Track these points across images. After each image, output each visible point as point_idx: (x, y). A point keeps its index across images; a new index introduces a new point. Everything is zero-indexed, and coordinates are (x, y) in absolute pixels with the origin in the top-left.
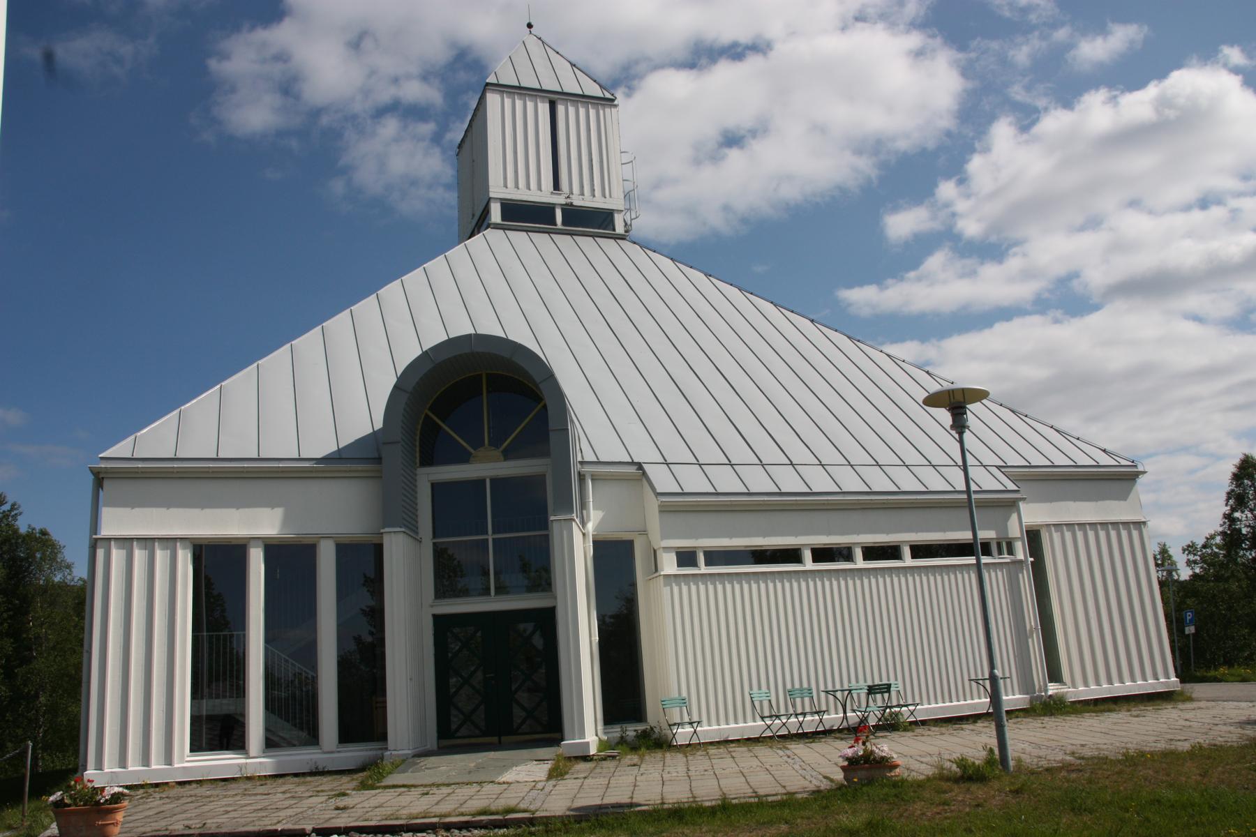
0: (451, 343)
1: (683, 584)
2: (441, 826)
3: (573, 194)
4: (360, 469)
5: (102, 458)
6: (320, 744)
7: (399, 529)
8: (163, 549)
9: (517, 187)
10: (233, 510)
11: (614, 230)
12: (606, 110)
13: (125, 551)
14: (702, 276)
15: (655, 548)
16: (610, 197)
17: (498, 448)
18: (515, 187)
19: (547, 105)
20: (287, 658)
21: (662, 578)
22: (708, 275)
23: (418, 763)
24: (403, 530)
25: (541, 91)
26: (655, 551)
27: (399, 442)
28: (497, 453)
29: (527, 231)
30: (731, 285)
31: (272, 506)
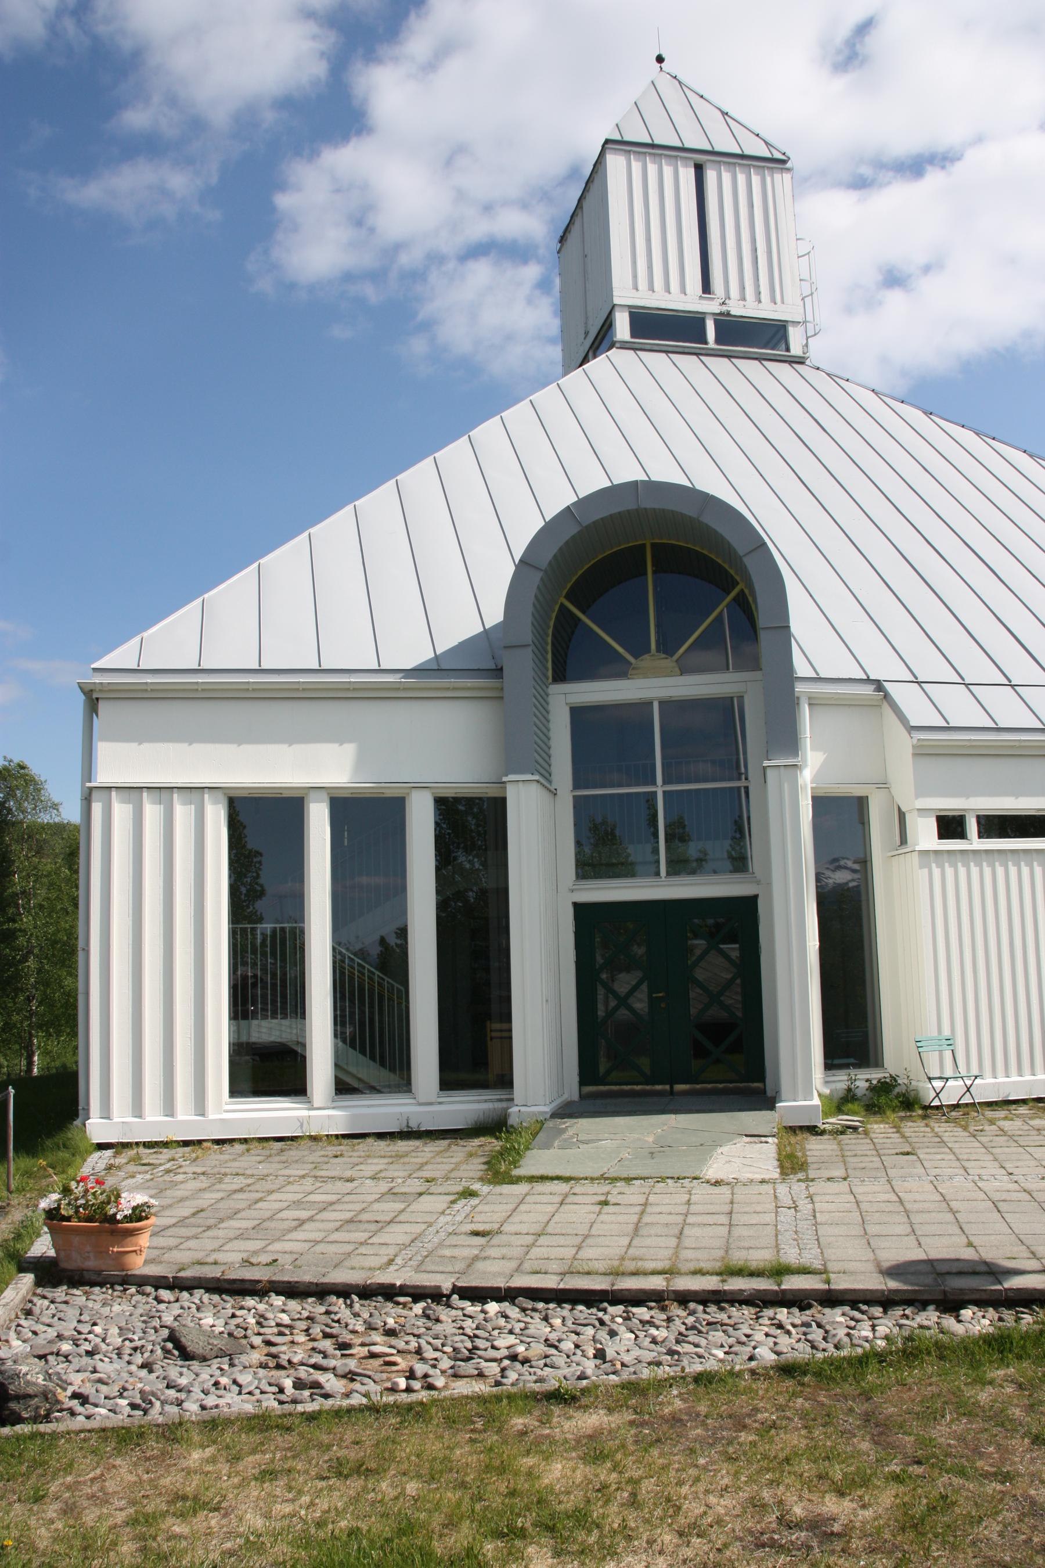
0: (583, 503)
1: (947, 865)
2: (672, 1296)
3: (729, 299)
4: (469, 685)
5: (95, 670)
6: (414, 1090)
7: (529, 777)
8: (184, 803)
9: (651, 288)
10: (284, 747)
11: (788, 350)
12: (775, 175)
13: (131, 806)
14: (920, 413)
15: (903, 809)
16: (783, 303)
17: (672, 656)
18: (649, 290)
19: (692, 171)
20: (352, 956)
21: (915, 855)
22: (929, 413)
23: (564, 1131)
24: (537, 777)
25: (683, 149)
26: (902, 816)
27: (529, 645)
28: (669, 663)
29: (667, 352)
30: (963, 426)
31: (340, 739)
